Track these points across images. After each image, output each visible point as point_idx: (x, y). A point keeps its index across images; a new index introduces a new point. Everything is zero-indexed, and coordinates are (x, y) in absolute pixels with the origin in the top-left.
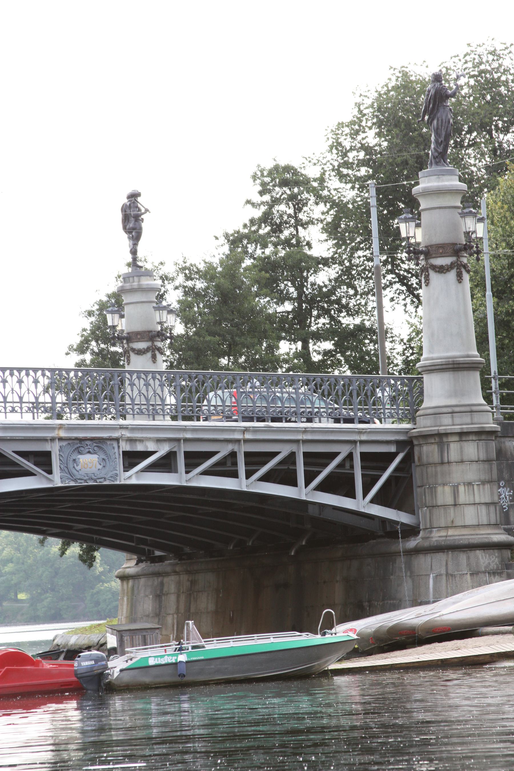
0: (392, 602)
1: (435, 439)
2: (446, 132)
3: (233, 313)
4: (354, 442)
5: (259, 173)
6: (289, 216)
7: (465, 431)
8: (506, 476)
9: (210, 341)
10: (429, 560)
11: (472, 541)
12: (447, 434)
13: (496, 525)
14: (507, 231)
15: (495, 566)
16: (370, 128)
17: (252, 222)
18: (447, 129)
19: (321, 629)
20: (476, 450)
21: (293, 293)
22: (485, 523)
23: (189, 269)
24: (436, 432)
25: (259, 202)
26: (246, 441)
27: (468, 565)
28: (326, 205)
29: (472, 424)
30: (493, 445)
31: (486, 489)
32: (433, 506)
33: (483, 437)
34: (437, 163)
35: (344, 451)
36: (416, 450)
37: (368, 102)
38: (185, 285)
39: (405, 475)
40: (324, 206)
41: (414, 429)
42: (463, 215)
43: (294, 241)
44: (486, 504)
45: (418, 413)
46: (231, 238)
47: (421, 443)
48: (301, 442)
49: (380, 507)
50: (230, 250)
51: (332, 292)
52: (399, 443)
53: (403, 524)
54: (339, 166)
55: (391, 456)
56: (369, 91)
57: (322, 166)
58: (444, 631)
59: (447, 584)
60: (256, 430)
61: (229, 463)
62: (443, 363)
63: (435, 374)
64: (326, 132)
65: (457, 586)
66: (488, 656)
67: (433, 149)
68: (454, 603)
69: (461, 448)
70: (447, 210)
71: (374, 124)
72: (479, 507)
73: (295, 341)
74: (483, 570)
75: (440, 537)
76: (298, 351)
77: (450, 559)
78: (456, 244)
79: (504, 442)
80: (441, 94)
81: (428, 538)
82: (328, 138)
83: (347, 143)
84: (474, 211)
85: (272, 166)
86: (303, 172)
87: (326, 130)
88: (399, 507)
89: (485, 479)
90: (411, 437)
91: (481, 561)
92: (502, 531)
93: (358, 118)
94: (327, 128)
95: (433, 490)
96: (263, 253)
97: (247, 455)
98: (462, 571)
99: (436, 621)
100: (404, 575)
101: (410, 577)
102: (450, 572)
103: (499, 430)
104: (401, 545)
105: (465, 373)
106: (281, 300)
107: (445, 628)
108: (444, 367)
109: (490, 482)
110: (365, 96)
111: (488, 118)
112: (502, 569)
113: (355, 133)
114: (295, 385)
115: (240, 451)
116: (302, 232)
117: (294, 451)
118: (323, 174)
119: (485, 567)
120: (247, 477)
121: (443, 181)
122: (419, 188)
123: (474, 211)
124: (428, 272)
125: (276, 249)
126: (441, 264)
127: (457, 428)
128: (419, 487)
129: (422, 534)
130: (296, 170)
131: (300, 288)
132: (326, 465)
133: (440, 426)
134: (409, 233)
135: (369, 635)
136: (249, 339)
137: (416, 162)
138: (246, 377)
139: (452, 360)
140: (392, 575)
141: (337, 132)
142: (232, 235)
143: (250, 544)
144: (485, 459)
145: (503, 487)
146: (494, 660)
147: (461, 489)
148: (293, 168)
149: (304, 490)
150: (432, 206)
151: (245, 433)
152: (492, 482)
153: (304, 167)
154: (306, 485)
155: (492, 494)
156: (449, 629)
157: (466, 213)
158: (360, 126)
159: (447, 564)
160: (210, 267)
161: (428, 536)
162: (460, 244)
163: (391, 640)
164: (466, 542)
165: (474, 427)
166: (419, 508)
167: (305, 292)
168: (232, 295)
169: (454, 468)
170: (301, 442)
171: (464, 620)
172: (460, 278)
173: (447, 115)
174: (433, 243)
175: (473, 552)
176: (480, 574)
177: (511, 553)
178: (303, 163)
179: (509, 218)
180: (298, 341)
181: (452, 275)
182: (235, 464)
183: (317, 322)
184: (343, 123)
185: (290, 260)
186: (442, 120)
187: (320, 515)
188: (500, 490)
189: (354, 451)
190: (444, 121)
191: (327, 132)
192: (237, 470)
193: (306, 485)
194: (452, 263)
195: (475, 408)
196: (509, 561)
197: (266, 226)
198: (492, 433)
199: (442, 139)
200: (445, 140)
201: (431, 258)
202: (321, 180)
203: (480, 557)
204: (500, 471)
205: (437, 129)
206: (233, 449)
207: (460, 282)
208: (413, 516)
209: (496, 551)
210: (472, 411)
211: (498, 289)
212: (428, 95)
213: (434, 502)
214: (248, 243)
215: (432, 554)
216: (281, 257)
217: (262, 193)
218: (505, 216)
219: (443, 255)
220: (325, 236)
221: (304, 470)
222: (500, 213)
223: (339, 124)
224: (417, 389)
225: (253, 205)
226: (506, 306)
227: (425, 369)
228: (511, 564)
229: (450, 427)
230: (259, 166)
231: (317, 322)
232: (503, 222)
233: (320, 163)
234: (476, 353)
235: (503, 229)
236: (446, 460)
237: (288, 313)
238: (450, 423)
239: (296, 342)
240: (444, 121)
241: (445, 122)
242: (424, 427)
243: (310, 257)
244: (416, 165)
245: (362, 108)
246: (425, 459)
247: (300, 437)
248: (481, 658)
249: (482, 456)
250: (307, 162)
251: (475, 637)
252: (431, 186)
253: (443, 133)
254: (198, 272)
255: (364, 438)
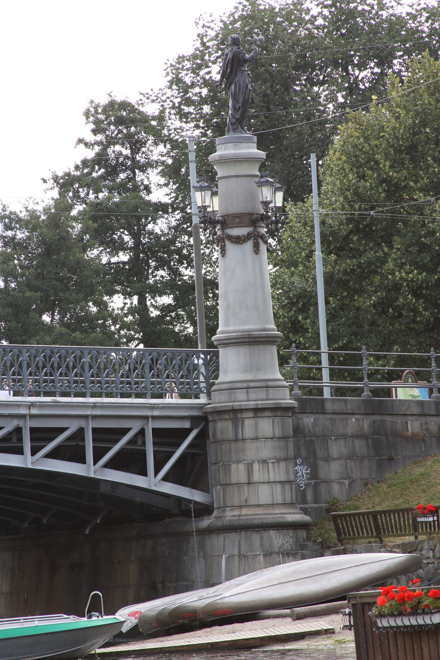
0: (185, 583)
1: (229, 415)
2: (244, 98)
3: (57, 266)
4: (146, 418)
5: (92, 110)
6: (126, 157)
7: (260, 407)
8: (303, 453)
9: (30, 297)
10: (222, 540)
11: (265, 521)
12: (241, 410)
13: (291, 504)
14: (344, 184)
15: (289, 547)
16: (214, 62)
17: (85, 163)
18: (245, 95)
19: (89, 612)
20: (271, 427)
21: (128, 242)
22: (280, 501)
23: (9, 218)
24: (231, 408)
25: (93, 142)
26: (32, 416)
27: (262, 545)
28: (165, 147)
29: (268, 400)
30: (289, 421)
31: (281, 467)
32: (227, 485)
33: (279, 413)
34: (234, 130)
35: (136, 426)
36: (211, 425)
37: (212, 33)
38: (5, 235)
39: (200, 452)
40: (163, 147)
41: (209, 404)
42: (260, 184)
43: (130, 185)
44: (281, 482)
45: (214, 388)
46: (61, 181)
47: (216, 419)
48: (90, 417)
49: (172, 485)
50: (60, 194)
51: (172, 242)
52: (192, 419)
53: (196, 502)
54: (180, 103)
55: (185, 433)
56: (212, 21)
57: (162, 103)
58: (226, 615)
59: (239, 565)
60: (42, 405)
61: (14, 439)
62: (239, 337)
63: (231, 347)
64: (165, 67)
65: (249, 567)
66: (258, 640)
67: (230, 115)
68: (238, 585)
69: (256, 424)
70: (244, 179)
71: (218, 57)
72: (273, 485)
73: (130, 295)
74: (277, 550)
75: (233, 516)
76: (134, 306)
77: (243, 539)
78: (253, 214)
79: (302, 418)
80: (239, 58)
81: (221, 517)
82: (168, 73)
83: (188, 80)
84: (270, 180)
85: (107, 102)
86: (141, 109)
87: (166, 64)
88: (194, 486)
89: (281, 457)
90: (205, 413)
91: (275, 541)
92: (299, 511)
93: (200, 51)
94: (167, 62)
95: (227, 468)
96: (97, 197)
97: (33, 430)
98: (255, 552)
99: (217, 604)
100: (197, 555)
101: (204, 557)
102: (243, 552)
103: (297, 406)
104: (194, 525)
105: (261, 347)
106: (114, 252)
107: (226, 611)
108: (240, 340)
109: (286, 459)
110: (209, 27)
111: (341, 54)
112: (296, 550)
113: (195, 70)
114: (84, 358)
115: (25, 427)
116: (140, 176)
117: (82, 426)
118: (162, 111)
119: (279, 548)
120: (33, 454)
121: (240, 148)
122: (216, 155)
123: (270, 180)
124: (224, 242)
125: (111, 195)
126: (237, 235)
127: (252, 404)
128: (214, 464)
129: (215, 513)
130: (133, 106)
131: (136, 236)
132: (116, 441)
133: (235, 402)
134: (205, 202)
135: (152, 618)
136: (73, 295)
137: (264, 102)
138: (33, 350)
139: (248, 333)
140: (186, 555)
141: (177, 66)
142: (62, 178)
143: (45, 522)
144: (281, 436)
145: (300, 465)
146: (265, 643)
147: (256, 466)
148: (129, 104)
149: (92, 468)
150: (229, 175)
151: (31, 408)
152: (287, 459)
153: (142, 104)
154: (95, 463)
155: (287, 472)
156: (231, 613)
157: (263, 182)
158: (203, 59)
159: (240, 545)
160: (33, 214)
161: (221, 515)
162: (257, 214)
163: (174, 624)
164: (260, 522)
165: (270, 403)
166: (213, 486)
167: (142, 241)
168: (56, 246)
169: (249, 445)
170: (90, 417)
171: (246, 602)
172: (256, 249)
173: (245, 80)
174: (230, 212)
175: (266, 532)
176: (273, 555)
177: (307, 534)
178: (141, 100)
179: (347, 170)
180: (134, 295)
181: (249, 246)
182: (20, 440)
183: (154, 274)
184: (184, 57)
185: (125, 207)
186: (240, 85)
187: (112, 492)
188: (297, 468)
189: (145, 427)
190: (242, 86)
191: (166, 66)
192: (22, 447)
193: (95, 463)
194: (248, 234)
195: (270, 384)
196: (304, 542)
197: (99, 169)
198: (288, 409)
199: (240, 105)
200: (243, 106)
201: (227, 228)
202: (161, 118)
203: (274, 538)
204: (297, 448)
205: (235, 94)
206: (18, 425)
207: (257, 253)
208: (207, 494)
209: (290, 531)
210: (267, 387)
211: (336, 246)
212: (226, 59)
213: (228, 481)
214: (79, 187)
215: (225, 534)
216: (115, 202)
217: (95, 132)
218: (343, 168)
219: (240, 225)
220: (162, 181)
221: (93, 446)
222: (338, 165)
223: (179, 57)
224: (213, 363)
225: (86, 144)
226: (344, 265)
227: (220, 342)
228: (306, 545)
229: (244, 403)
230: (92, 102)
231: (154, 274)
232: (342, 174)
233: (159, 100)
234: (274, 327)
235: (341, 181)
236: (240, 437)
237: (124, 263)
238: (245, 398)
239: (132, 296)
240: (242, 86)
241: (243, 88)
242: (219, 403)
243: (149, 203)
244: (262, 104)
245: (205, 40)
246: (219, 436)
247: (89, 412)
248: (251, 642)
249: (278, 433)
250: (144, 99)
251: (255, 620)
252: (228, 154)
253: (241, 99)
254: (19, 220)
255: (156, 413)
